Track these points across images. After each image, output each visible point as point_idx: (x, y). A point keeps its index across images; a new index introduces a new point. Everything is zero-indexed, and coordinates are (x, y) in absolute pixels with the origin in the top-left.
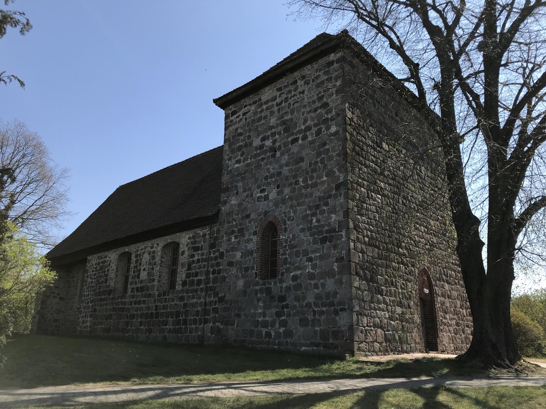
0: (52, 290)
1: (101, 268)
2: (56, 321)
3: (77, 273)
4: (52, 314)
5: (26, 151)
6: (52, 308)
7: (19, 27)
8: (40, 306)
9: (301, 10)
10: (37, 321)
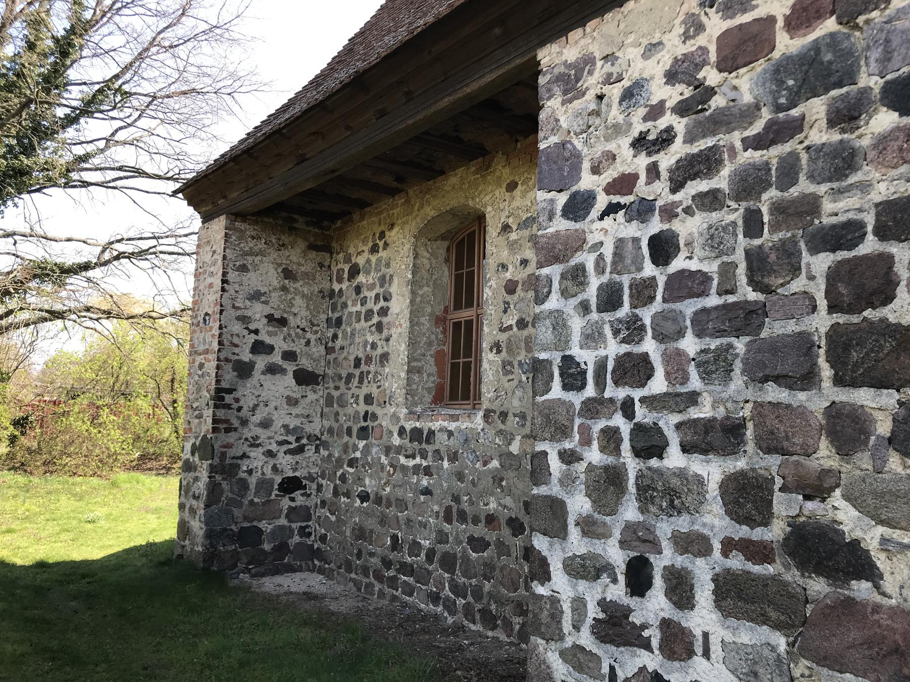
0: (256, 332)
1: (693, 523)
2: (291, 485)
3: (374, 250)
4: (270, 454)
5: (868, 470)
6: (266, 424)
7: (530, 325)
8: (208, 413)
9: (190, 221)
10: (201, 487)
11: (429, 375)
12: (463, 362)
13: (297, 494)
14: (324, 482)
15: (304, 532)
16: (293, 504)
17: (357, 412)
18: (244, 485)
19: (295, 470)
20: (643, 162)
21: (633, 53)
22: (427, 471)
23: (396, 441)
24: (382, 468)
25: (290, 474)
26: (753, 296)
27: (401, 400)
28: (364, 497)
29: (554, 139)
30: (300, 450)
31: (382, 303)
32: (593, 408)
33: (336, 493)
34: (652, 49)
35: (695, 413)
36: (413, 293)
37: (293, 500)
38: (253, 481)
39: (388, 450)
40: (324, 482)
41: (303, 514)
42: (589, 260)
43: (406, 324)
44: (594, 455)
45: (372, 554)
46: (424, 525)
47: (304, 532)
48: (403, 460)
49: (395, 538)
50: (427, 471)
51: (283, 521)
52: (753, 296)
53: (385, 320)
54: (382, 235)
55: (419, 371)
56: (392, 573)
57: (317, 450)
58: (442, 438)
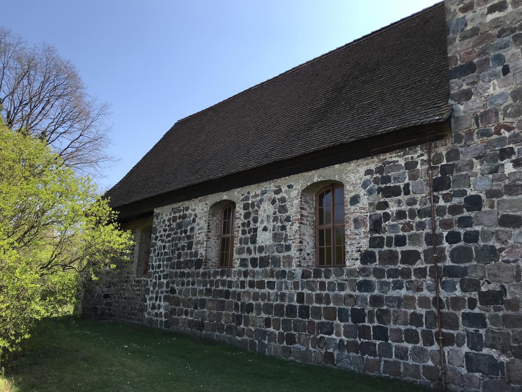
2: (106, 296)
11: (143, 267)
12: (324, 248)
13: (108, 299)
14: (116, 296)
15: (109, 309)
16: (107, 301)
17: (125, 276)
18: (93, 296)
19: (108, 292)
20: (164, 233)
21: (164, 215)
22: (139, 290)
23: (133, 283)
24: (130, 290)
25: (107, 293)
26: (171, 256)
27: (135, 273)
28: (125, 298)
29: (154, 226)
30: (109, 287)
31: (133, 247)
32: (155, 273)
33: (119, 298)
34: (167, 215)
35: (165, 273)
36: (140, 245)
37: (107, 300)
38: (96, 295)
39: (132, 286)
40: (116, 296)
41: (110, 304)
42: (156, 247)
43: (138, 254)
44: (154, 280)
45: (126, 313)
46: (137, 303)
47: (109, 309)
48: (134, 288)
49: (131, 307)
50: (139, 290)
51: (104, 306)
52: (171, 256)
53: (134, 252)
54: (134, 229)
55: (140, 265)
56: (130, 316)
57: (114, 287)
58: (143, 282)
